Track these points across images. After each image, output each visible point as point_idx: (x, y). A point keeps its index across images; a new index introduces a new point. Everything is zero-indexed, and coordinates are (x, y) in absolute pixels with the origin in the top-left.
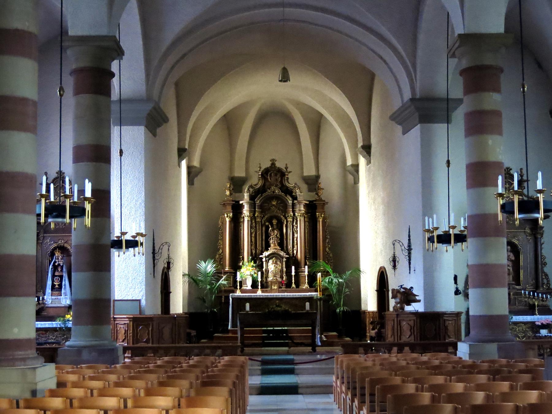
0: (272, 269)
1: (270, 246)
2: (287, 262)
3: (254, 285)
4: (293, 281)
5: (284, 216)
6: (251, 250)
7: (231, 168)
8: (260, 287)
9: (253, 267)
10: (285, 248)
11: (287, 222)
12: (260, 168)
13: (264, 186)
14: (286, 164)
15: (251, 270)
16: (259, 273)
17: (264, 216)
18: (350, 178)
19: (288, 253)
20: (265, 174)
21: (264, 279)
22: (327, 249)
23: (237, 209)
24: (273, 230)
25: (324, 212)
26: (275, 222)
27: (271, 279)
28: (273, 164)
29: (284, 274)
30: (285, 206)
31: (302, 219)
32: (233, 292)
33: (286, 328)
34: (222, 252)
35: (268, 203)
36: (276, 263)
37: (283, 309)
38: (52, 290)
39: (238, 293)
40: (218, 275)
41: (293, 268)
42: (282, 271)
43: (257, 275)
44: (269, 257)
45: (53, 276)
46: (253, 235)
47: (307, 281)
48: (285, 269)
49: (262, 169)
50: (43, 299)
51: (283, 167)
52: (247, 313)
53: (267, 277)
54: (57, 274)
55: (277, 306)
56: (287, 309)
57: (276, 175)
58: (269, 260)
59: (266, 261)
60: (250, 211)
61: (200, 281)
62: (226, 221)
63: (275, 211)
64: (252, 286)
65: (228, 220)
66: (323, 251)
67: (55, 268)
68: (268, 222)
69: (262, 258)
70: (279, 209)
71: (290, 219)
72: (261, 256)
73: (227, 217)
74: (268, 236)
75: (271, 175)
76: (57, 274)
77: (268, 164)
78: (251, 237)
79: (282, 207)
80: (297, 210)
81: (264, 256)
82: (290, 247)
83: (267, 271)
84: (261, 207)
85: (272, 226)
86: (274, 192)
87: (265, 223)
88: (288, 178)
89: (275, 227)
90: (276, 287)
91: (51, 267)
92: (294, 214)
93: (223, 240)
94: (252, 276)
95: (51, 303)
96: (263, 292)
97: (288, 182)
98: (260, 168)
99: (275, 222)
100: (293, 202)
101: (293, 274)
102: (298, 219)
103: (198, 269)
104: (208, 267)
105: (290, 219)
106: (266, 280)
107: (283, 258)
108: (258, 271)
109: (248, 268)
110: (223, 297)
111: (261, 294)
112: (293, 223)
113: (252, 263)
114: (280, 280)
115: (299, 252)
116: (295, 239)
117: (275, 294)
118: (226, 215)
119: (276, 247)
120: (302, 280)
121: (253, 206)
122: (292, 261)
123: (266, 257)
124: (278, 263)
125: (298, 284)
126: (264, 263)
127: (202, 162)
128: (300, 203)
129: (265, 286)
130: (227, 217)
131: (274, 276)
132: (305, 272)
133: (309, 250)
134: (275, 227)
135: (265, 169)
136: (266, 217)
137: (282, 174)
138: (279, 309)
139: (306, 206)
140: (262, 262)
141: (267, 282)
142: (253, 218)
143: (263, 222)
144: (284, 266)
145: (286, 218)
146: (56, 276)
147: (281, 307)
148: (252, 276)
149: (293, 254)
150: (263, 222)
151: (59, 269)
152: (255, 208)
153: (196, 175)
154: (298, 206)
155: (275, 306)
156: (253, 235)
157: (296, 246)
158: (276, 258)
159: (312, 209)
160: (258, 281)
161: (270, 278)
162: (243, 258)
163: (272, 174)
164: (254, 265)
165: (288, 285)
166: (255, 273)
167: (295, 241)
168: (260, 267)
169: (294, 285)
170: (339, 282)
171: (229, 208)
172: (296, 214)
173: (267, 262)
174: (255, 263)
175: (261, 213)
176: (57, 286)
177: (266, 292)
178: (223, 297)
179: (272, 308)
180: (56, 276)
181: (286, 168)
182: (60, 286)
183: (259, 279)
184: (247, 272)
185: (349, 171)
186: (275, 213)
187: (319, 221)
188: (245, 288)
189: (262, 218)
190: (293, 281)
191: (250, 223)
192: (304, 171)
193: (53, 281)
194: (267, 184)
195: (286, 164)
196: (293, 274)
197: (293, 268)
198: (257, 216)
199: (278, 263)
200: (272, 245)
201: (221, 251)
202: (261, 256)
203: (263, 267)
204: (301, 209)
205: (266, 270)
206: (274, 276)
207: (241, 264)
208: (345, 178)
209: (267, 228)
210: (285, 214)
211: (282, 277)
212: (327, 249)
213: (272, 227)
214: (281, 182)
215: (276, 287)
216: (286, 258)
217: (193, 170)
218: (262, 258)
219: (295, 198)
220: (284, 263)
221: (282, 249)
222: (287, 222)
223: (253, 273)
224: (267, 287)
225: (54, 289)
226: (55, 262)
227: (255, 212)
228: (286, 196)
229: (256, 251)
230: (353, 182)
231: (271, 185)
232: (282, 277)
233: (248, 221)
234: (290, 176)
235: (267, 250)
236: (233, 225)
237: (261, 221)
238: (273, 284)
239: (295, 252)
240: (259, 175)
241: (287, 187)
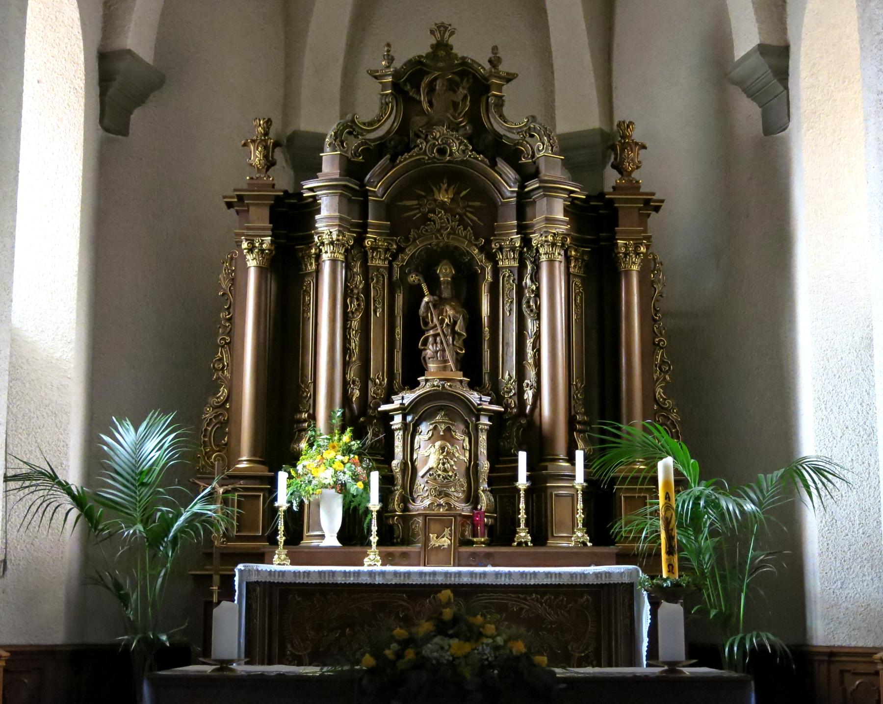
0: (432, 463)
1: (422, 371)
2: (493, 435)
3: (353, 531)
4: (522, 515)
5: (486, 250)
6: (345, 384)
7: (288, 102)
8: (374, 539)
9: (347, 451)
10: (486, 378)
11: (496, 271)
12: (391, 60)
13: (404, 128)
14: (495, 49)
15: (338, 466)
16: (375, 476)
17: (401, 250)
18: (748, 112)
19: (498, 399)
20: (408, 83)
21: (396, 505)
22: (659, 391)
23: (291, 220)
24: (438, 305)
25: (648, 238)
26: (445, 272)
27: (427, 502)
28: (441, 47)
29: (484, 485)
30: (490, 210)
31: (560, 258)
32: (261, 557)
34: (227, 400)
35: (419, 198)
36: (448, 436)
37: (485, 648)
39: (280, 565)
40: (186, 474)
41: (522, 456)
42: (472, 471)
43: (367, 485)
44: (419, 411)
46: (355, 324)
47: (580, 516)
48: (485, 465)
49: (398, 64)
51: (481, 58)
52: (224, 681)
53: (408, 497)
55: (442, 629)
56: (519, 647)
57: (452, 86)
58: (417, 424)
59: (405, 426)
60: (344, 225)
61: (112, 506)
62: (246, 269)
63: (444, 230)
64: (341, 536)
65: (252, 262)
66: (645, 397)
68: (417, 271)
69: (387, 417)
70: (461, 222)
71: (508, 262)
72: (384, 408)
73: (251, 250)
74: (415, 329)
75: (431, 88)
77: (419, 46)
78: (346, 329)
79: (476, 211)
80: (538, 220)
81: (396, 404)
82: (508, 373)
83: (410, 468)
84: (389, 210)
85: (434, 285)
86: (442, 152)
87: (404, 275)
88: (500, 103)
89: (446, 293)
90: (445, 541)
92: (526, 241)
93: (233, 346)
94: (342, 488)
96: (387, 559)
97: (501, 116)
98: (391, 60)
99: (445, 272)
100: (522, 187)
101: (522, 482)
102: (543, 258)
103: (107, 456)
104: (144, 443)
105: (508, 262)
106: (406, 509)
107: (477, 412)
108: (369, 470)
109: (329, 454)
110: (216, 579)
111: (379, 568)
112: (521, 278)
113: (346, 437)
114: (465, 509)
115: (549, 394)
116: (529, 342)
117: (438, 566)
118: (245, 245)
119: (448, 375)
120: (559, 512)
121: (355, 199)
122: (513, 429)
123: (404, 411)
124: (459, 436)
125: (541, 533)
126: (398, 436)
127: (162, 45)
128: (548, 190)
129: (396, 534)
130: (251, 250)
131: (441, 494)
132: (573, 477)
133: (586, 391)
134: (446, 293)
135: (410, 63)
136: (409, 252)
137: (477, 87)
138: (457, 647)
139: (574, 209)
140: (390, 434)
141: (407, 518)
142: (355, 253)
143: (397, 274)
144: (483, 450)
145: (492, 258)
147: (474, 635)
148: (342, 488)
149: (522, 403)
150: (397, 274)
152: (365, 216)
153: (140, 99)
154: (542, 205)
155: (425, 627)
156: (355, 324)
157: (531, 373)
158: (451, 415)
159: (599, 230)
160: (367, 511)
161: (422, 503)
162: (313, 417)
163: (438, 85)
164: (355, 445)
165: (501, 533)
166: (355, 478)
167: (530, 352)
168: (380, 454)
169: (523, 534)
170: (743, 512)
171: (260, 217)
172: (536, 239)
173: (411, 431)
174: (358, 435)
175: (393, 232)
177: (405, 559)
178: (216, 579)
179: (409, 642)
181: (494, 62)
183: (374, 504)
184: (324, 473)
185: (740, 83)
186: (445, 239)
187: (628, 273)
188: (315, 543)
189: (395, 256)
190: (522, 515)
191: (341, 274)
192: (559, 113)
194: (418, 121)
195: (495, 49)
196: (522, 482)
197: (522, 456)
198: (374, 249)
199: (459, 436)
200: (432, 366)
201: (223, 392)
202: (384, 408)
203: (392, 457)
204: (553, 216)
205: (404, 464)
206: (441, 494)
207: (303, 445)
208: (722, 113)
209: (414, 295)
210: (488, 242)
211: (472, 498)
212: (659, 391)
213: (432, 293)
214: (474, 118)
215: (445, 541)
216: (494, 416)
217: (121, 66)
218: (387, 417)
219: (527, 173)
220: (483, 438)
221: (475, 384)
222: (496, 271)
223: (346, 478)
224: (406, 541)
227: (363, 227)
228: (493, 165)
229: (364, 390)
230: (758, 127)
231: (430, 125)
232: (472, 498)
233: (334, 261)
234: (508, 91)
235: (412, 384)
236: (273, 287)
237: (390, 269)
238: (434, 526)
239: (529, 395)
240: (384, 86)
241: (498, 137)
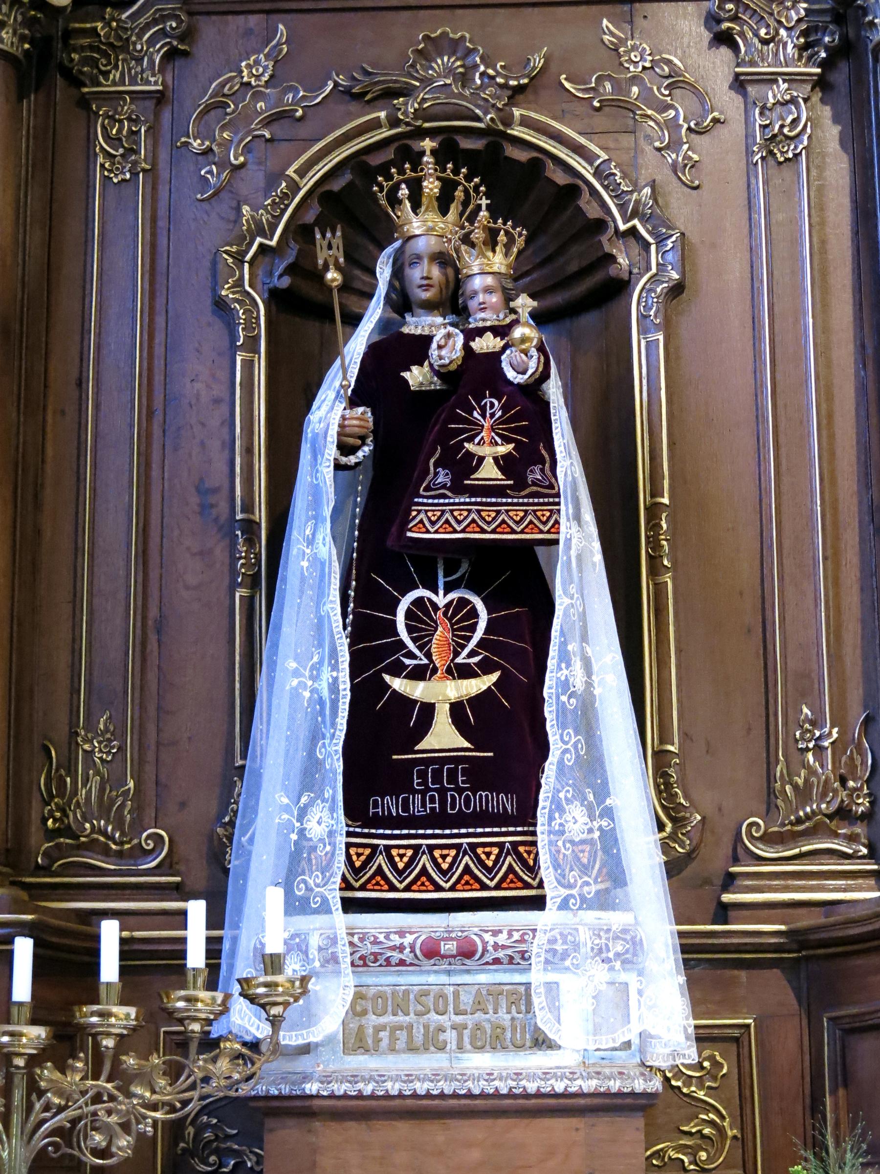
33: (826, 1024)
38: (356, 809)
45: (379, 564)
50: (153, 965)
54: (434, 520)
67: (410, 430)
76: (434, 520)
91: (329, 413)
95: (357, 1041)
146: (428, 561)
151: (489, 452)
176: (443, 736)
180: (428, 561)
182: (510, 738)
193: (372, 650)
225: (398, 781)
226: (394, 351)
